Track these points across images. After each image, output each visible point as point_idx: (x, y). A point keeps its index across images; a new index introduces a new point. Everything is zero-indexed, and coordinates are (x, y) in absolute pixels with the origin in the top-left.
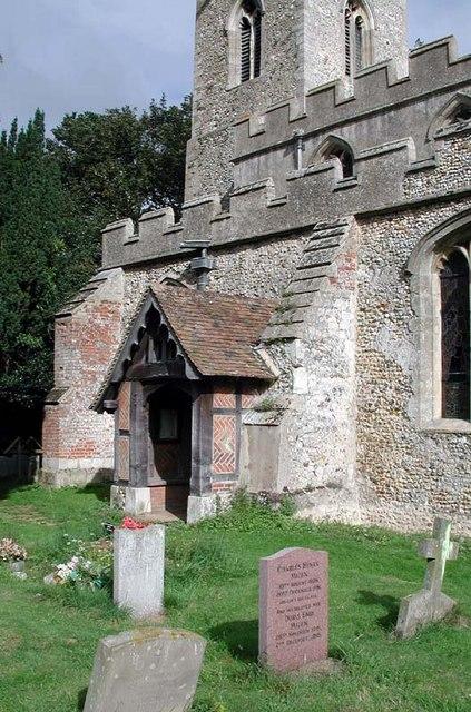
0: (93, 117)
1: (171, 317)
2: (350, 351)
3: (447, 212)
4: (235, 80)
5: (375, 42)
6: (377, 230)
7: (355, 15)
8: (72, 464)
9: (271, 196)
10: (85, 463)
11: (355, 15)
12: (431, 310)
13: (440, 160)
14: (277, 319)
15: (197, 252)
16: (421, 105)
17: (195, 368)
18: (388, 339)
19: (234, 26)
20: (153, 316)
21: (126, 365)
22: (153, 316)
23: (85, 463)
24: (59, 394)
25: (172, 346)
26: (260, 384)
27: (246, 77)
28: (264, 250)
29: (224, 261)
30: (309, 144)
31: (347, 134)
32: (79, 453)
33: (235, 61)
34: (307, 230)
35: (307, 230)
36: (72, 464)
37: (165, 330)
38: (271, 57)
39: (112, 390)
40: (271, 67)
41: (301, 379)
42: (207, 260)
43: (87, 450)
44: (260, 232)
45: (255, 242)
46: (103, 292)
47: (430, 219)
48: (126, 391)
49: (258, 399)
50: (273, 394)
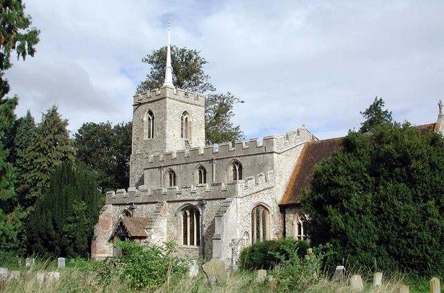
0: (94, 125)
1: (125, 224)
2: (165, 230)
3: (184, 203)
4: (146, 137)
5: (192, 125)
6: (171, 205)
7: (185, 117)
8: (100, 255)
9: (149, 193)
10: (103, 255)
11: (185, 117)
12: (181, 222)
13: (182, 192)
14: (148, 222)
15: (132, 204)
16: (192, 164)
17: (220, 214)
18: (173, 228)
19: (145, 119)
20: (121, 223)
21: (116, 233)
22: (121, 223)
23: (103, 255)
24: (96, 238)
25: (126, 230)
26: (145, 238)
27: (149, 137)
28: (148, 205)
29: (138, 206)
30: (165, 169)
31: (174, 168)
32: (102, 253)
33: (146, 131)
34: (157, 202)
35: (157, 202)
36: (100, 255)
37: (124, 226)
38: (157, 133)
39: (112, 238)
40: (157, 136)
41: (153, 237)
42: (134, 206)
43: (104, 252)
44: (147, 201)
45: (146, 203)
46: (107, 211)
47: (180, 204)
48: (116, 238)
49: (144, 240)
50: (147, 239)
